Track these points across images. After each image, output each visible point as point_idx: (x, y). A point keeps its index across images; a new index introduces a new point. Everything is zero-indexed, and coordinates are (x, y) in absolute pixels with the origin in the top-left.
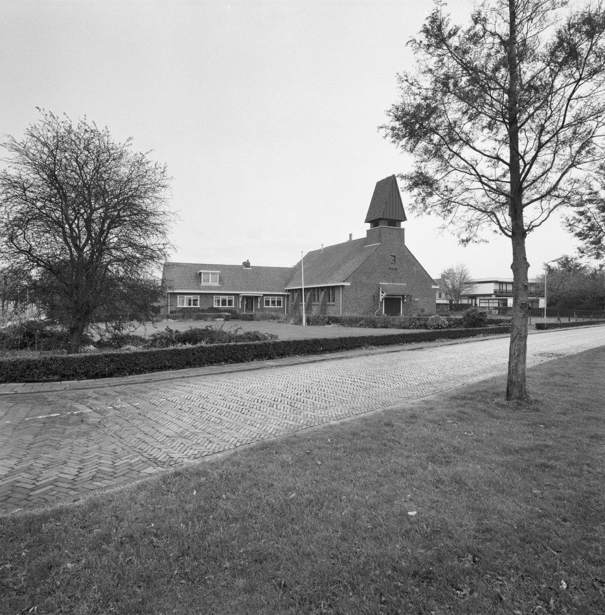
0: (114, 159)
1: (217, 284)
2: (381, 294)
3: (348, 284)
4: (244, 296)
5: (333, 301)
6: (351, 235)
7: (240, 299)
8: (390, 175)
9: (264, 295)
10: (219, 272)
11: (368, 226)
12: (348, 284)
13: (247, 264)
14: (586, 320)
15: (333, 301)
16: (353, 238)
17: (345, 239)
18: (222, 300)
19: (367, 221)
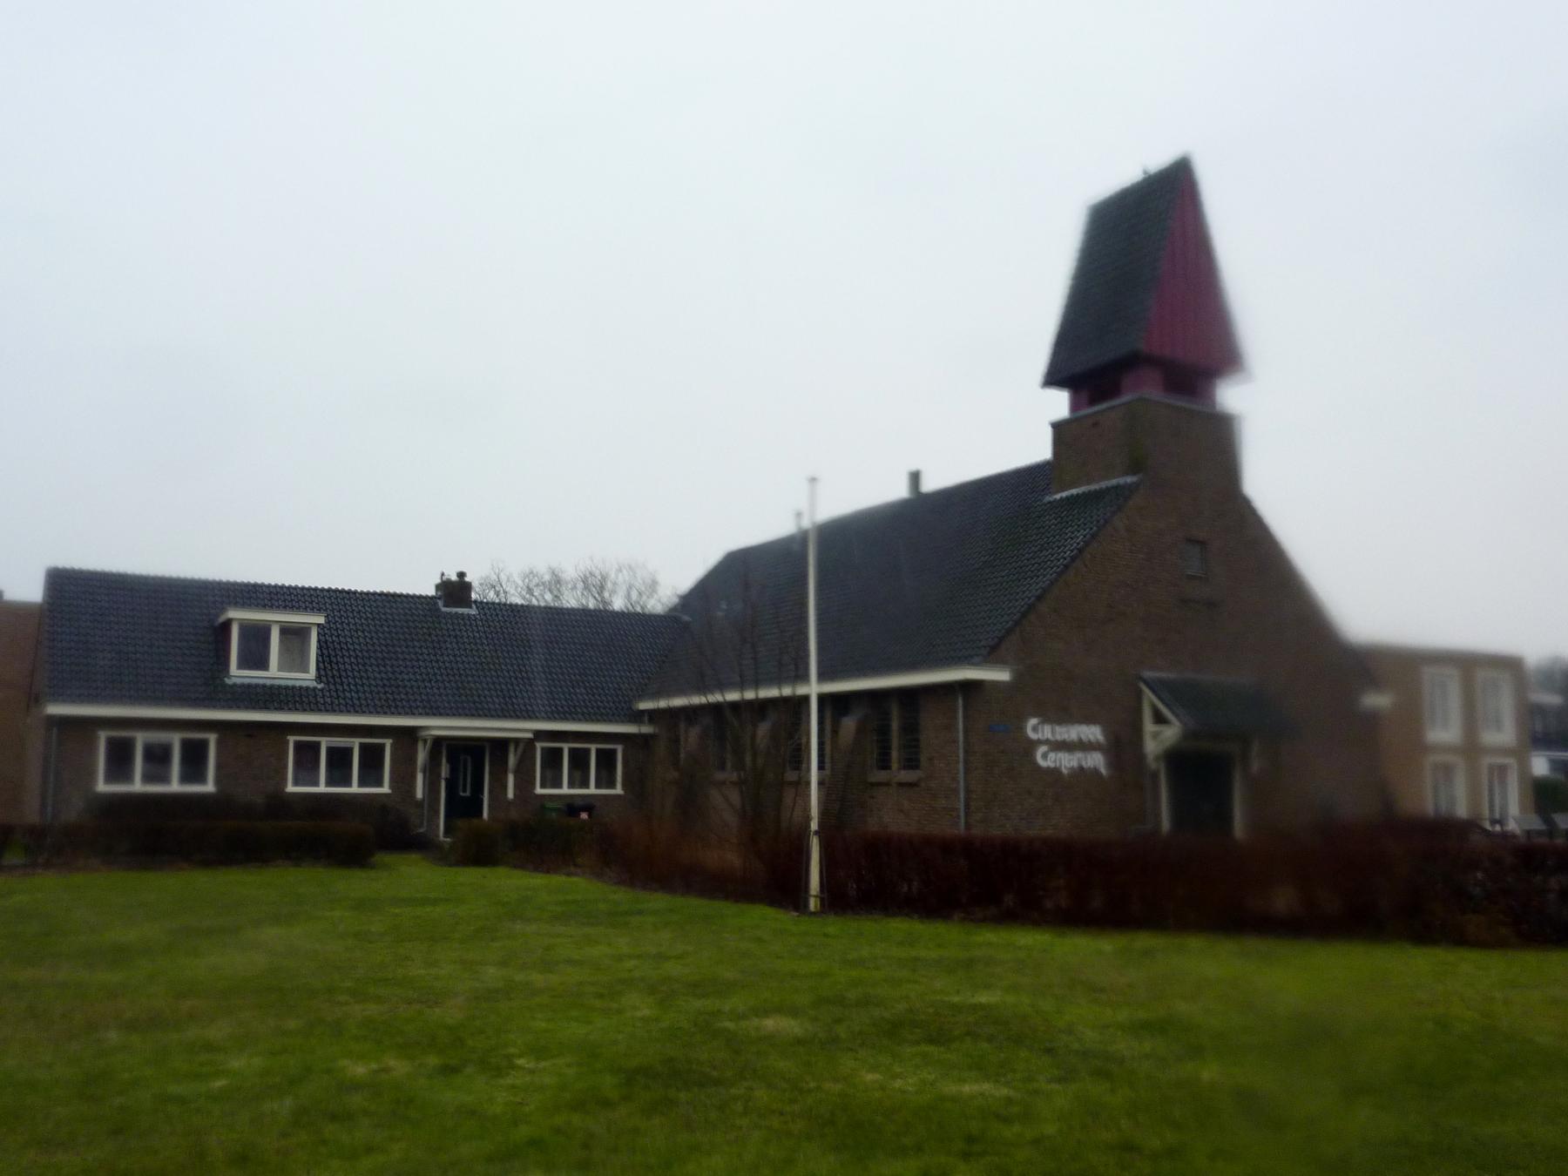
0: (782, 1114)
1: (307, 677)
2: (1149, 726)
3: (1001, 675)
4: (438, 741)
5: (911, 763)
6: (915, 478)
7: (422, 756)
8: (1158, 159)
9: (540, 735)
10: (321, 620)
11: (1059, 403)
12: (1001, 675)
13: (455, 590)
14: (462, 770)
15: (911, 763)
16: (930, 485)
17: (899, 491)
18: (332, 751)
19: (1054, 379)
